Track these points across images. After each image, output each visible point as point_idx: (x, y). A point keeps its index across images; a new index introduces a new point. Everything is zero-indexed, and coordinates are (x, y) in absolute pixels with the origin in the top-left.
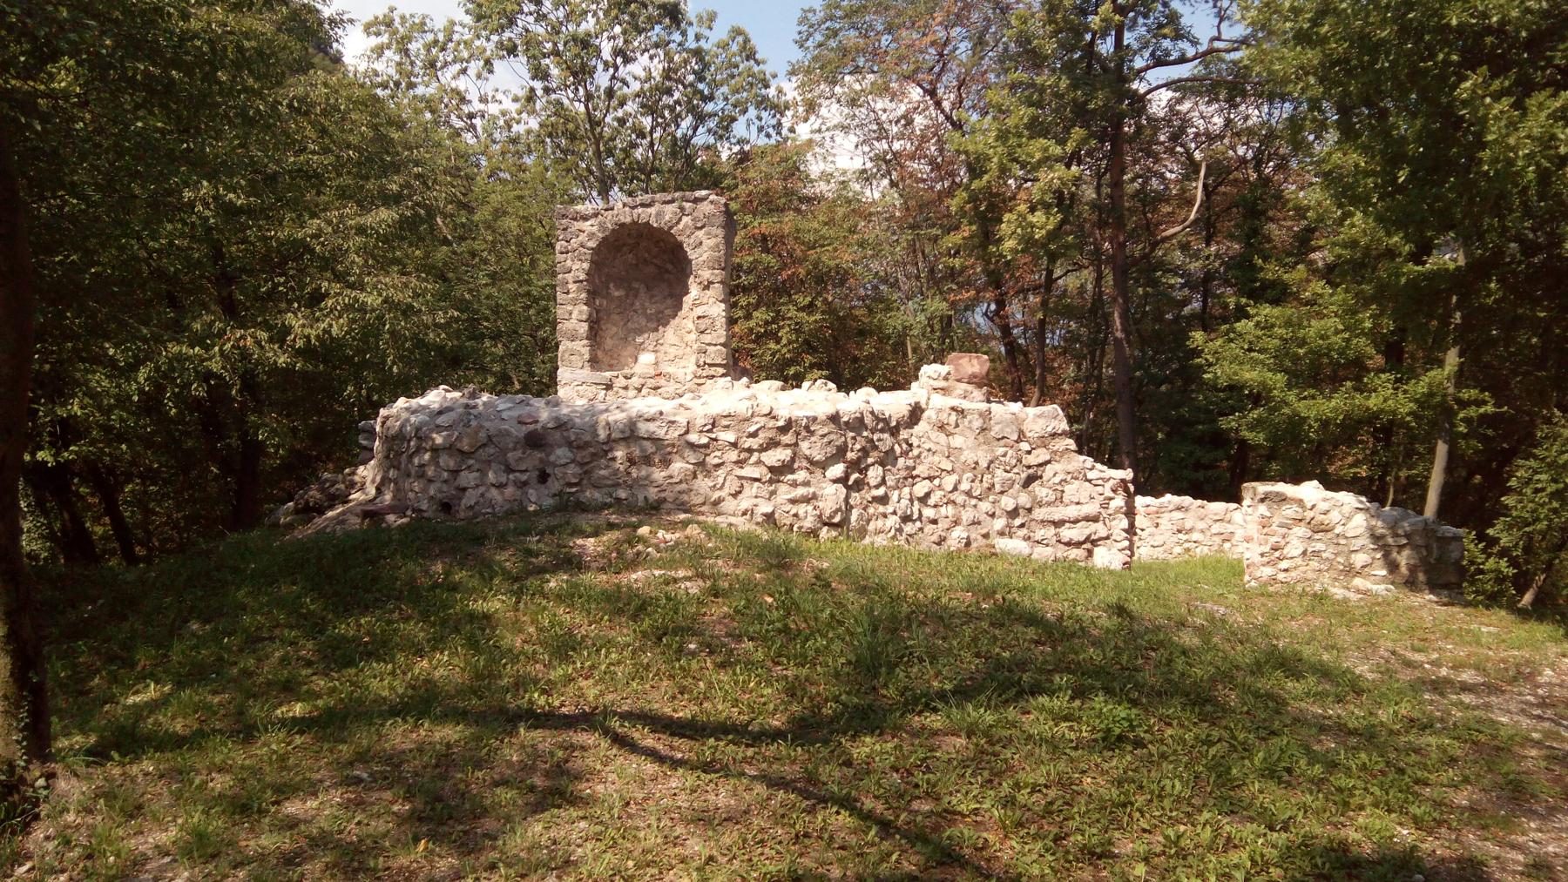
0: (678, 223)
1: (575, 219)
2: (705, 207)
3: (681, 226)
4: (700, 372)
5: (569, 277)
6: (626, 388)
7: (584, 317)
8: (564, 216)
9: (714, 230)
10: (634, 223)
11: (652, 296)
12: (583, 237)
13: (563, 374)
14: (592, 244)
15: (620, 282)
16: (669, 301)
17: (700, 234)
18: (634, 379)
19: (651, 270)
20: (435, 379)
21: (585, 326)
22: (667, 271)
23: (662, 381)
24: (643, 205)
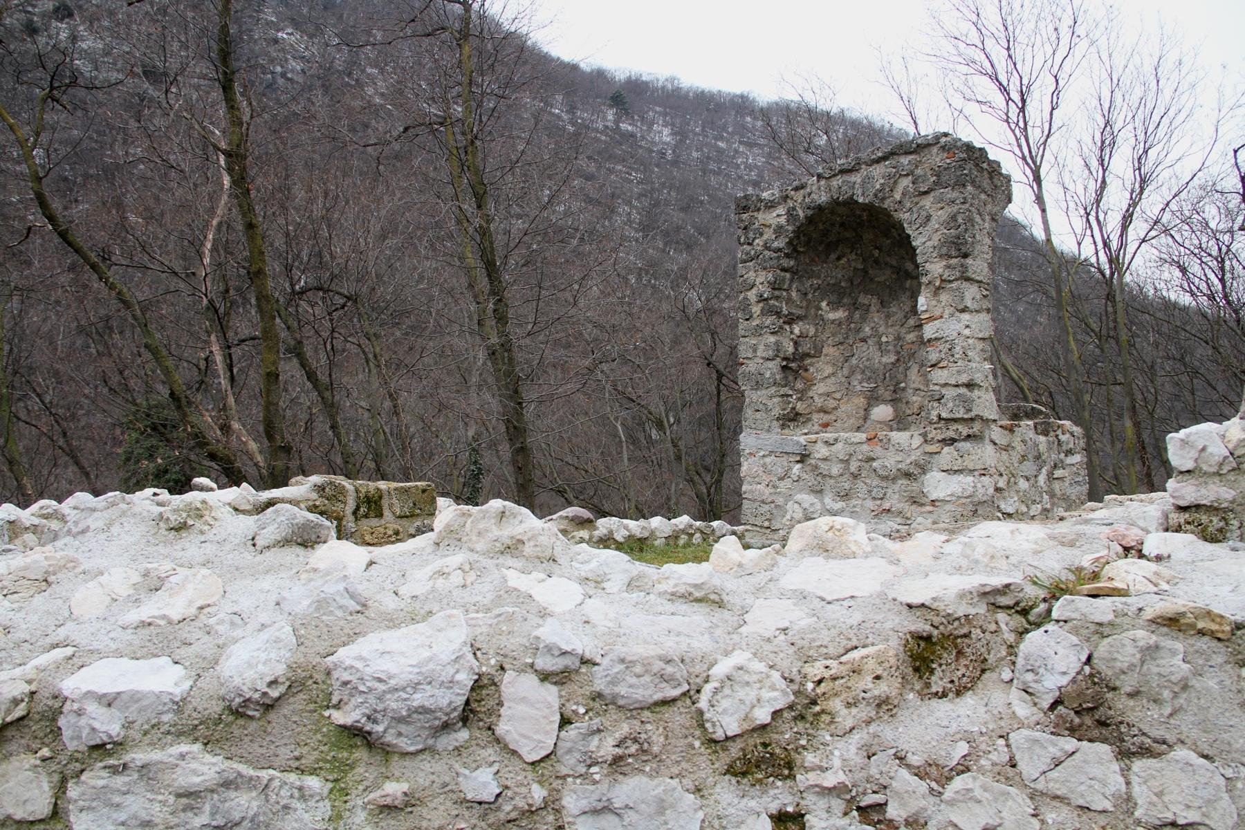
5: (752, 295)
10: (836, 202)
13: (747, 440)
15: (838, 295)
17: (927, 202)
18: (839, 446)
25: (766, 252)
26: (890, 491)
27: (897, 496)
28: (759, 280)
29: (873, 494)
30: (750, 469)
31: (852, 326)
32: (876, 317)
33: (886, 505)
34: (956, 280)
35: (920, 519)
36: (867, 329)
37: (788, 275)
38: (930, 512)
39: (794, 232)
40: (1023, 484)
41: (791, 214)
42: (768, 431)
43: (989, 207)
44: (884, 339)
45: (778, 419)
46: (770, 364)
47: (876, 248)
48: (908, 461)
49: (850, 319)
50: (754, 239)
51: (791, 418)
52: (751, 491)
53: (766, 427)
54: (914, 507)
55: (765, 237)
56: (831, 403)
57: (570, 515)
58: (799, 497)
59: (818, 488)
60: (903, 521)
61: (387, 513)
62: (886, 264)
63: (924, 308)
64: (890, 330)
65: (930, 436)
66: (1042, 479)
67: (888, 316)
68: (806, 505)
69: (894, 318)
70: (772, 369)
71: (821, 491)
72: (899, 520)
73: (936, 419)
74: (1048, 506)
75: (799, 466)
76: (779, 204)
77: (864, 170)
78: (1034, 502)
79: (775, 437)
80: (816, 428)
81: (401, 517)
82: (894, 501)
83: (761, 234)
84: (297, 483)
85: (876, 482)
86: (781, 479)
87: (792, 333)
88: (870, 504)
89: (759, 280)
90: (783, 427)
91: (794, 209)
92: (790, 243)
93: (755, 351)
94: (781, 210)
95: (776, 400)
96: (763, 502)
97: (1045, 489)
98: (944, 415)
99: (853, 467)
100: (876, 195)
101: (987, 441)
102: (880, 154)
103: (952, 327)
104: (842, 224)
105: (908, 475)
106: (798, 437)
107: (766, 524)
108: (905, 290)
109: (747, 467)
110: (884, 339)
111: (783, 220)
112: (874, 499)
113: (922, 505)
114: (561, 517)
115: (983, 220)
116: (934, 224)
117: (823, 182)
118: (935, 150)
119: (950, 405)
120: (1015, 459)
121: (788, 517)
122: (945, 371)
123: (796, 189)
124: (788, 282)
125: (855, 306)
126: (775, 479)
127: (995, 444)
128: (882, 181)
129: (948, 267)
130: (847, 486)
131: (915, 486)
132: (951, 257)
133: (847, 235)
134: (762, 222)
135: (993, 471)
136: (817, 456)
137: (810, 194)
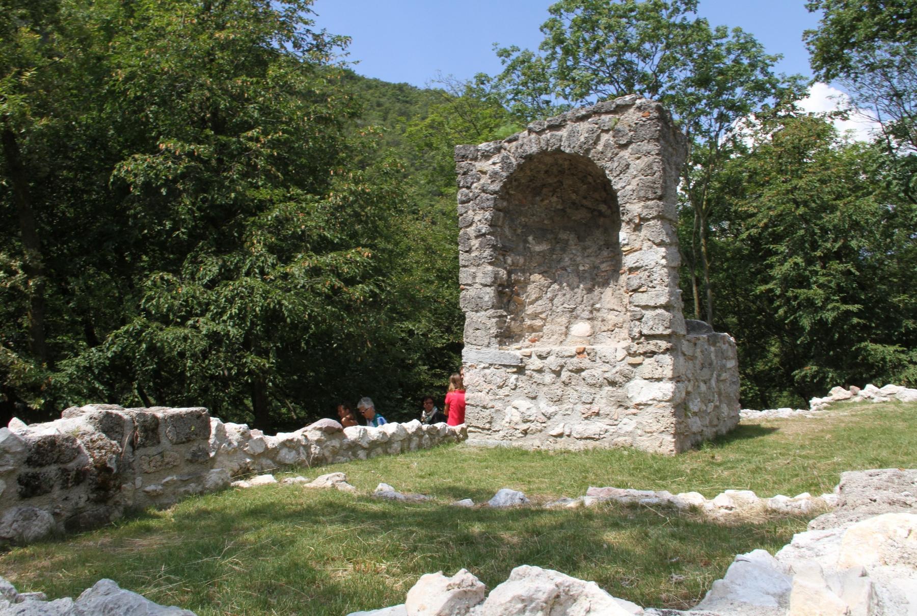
0: (596, 143)
1: (475, 159)
2: (632, 116)
3: (600, 148)
4: (635, 348)
5: (471, 231)
6: (540, 371)
7: (489, 280)
8: (464, 157)
9: (646, 146)
10: (543, 152)
11: (584, 249)
12: (485, 180)
13: (469, 354)
14: (496, 186)
15: (542, 233)
16: (605, 253)
17: (625, 153)
18: (551, 359)
19: (580, 215)
20: (534, 560)
21: (491, 291)
22: (601, 214)
23: (585, 362)
24: (552, 127)
25: (482, 194)
26: (598, 396)
27: (604, 401)
28: (477, 218)
29: (583, 399)
30: (472, 379)
31: (554, 256)
32: (574, 249)
33: (595, 408)
34: (653, 218)
35: (625, 420)
36: (567, 259)
37: (502, 214)
38: (634, 414)
39: (507, 177)
40: (703, 387)
41: (505, 160)
42: (488, 346)
43: (674, 158)
44: (581, 268)
45: (496, 337)
46: (488, 289)
47: (574, 192)
48: (614, 371)
49: (552, 251)
50: (472, 183)
51: (506, 336)
52: (473, 398)
53: (486, 342)
54: (620, 409)
55: (482, 181)
56: (538, 323)
57: (324, 426)
58: (516, 403)
59: (533, 395)
60: (611, 422)
61: (164, 441)
62: (582, 206)
63: (625, 242)
64: (587, 260)
65: (633, 349)
66: (713, 382)
67: (584, 249)
68: (523, 409)
69: (590, 251)
70: (489, 295)
71: (534, 398)
72: (607, 421)
73: (638, 335)
74: (718, 404)
75: (515, 376)
76: (494, 154)
77: (570, 125)
78: (710, 401)
79: (494, 352)
80: (527, 343)
81: (176, 444)
82: (602, 404)
83: (479, 179)
84: (71, 415)
85: (585, 389)
86: (501, 387)
87: (505, 263)
88: (580, 408)
89: (477, 218)
90: (501, 343)
91: (508, 158)
92: (504, 186)
93: (474, 277)
94: (496, 158)
95: (494, 320)
96: (484, 407)
97: (716, 390)
98: (645, 332)
99: (565, 375)
100: (581, 147)
101: (680, 353)
102: (584, 113)
103: (651, 257)
104: (546, 172)
105: (612, 383)
106: (514, 351)
107: (487, 426)
108: (598, 227)
109: (468, 377)
110: (581, 268)
111: (497, 168)
112: (584, 403)
113: (627, 408)
114: (315, 428)
115: (671, 169)
116: (632, 171)
117: (533, 136)
118: (632, 110)
119: (651, 323)
120: (698, 366)
121: (507, 419)
122: (645, 294)
123: (510, 141)
124: (501, 219)
125: (557, 241)
126: (494, 387)
127: (685, 355)
128: (587, 135)
129: (647, 207)
130: (559, 392)
131: (620, 392)
132: (648, 199)
133: (550, 181)
134: (479, 168)
135: (684, 378)
136: (532, 367)
137: (522, 145)
